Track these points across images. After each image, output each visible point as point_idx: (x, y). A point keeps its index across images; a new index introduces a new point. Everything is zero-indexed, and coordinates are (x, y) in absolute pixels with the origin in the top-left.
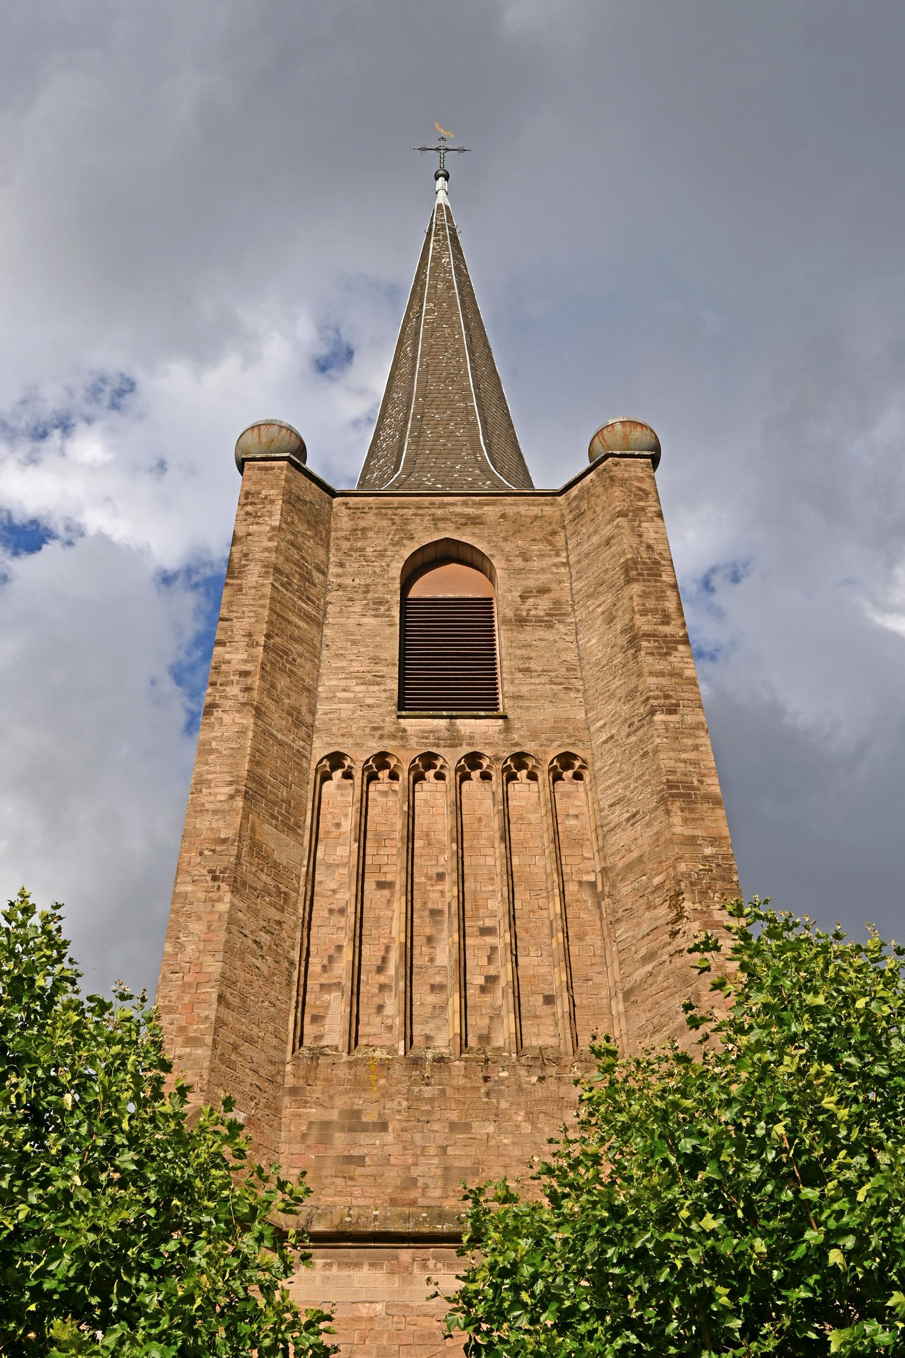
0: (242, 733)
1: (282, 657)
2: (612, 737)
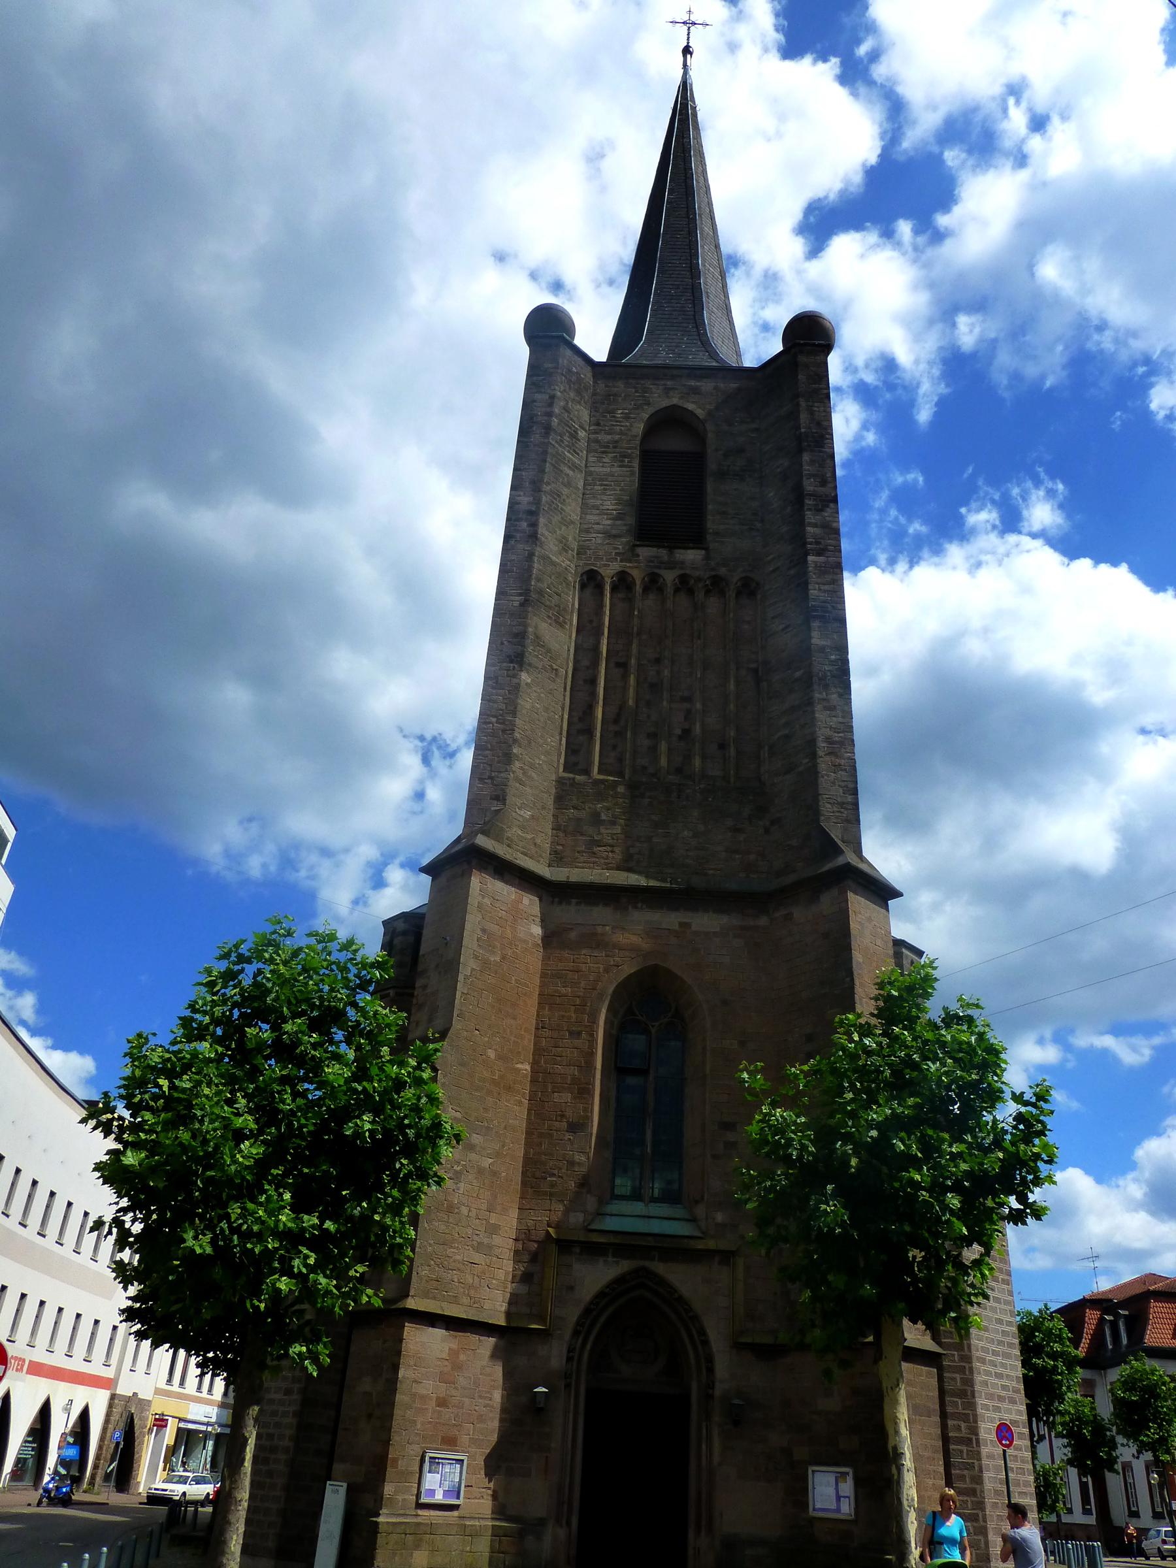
1: (556, 499)
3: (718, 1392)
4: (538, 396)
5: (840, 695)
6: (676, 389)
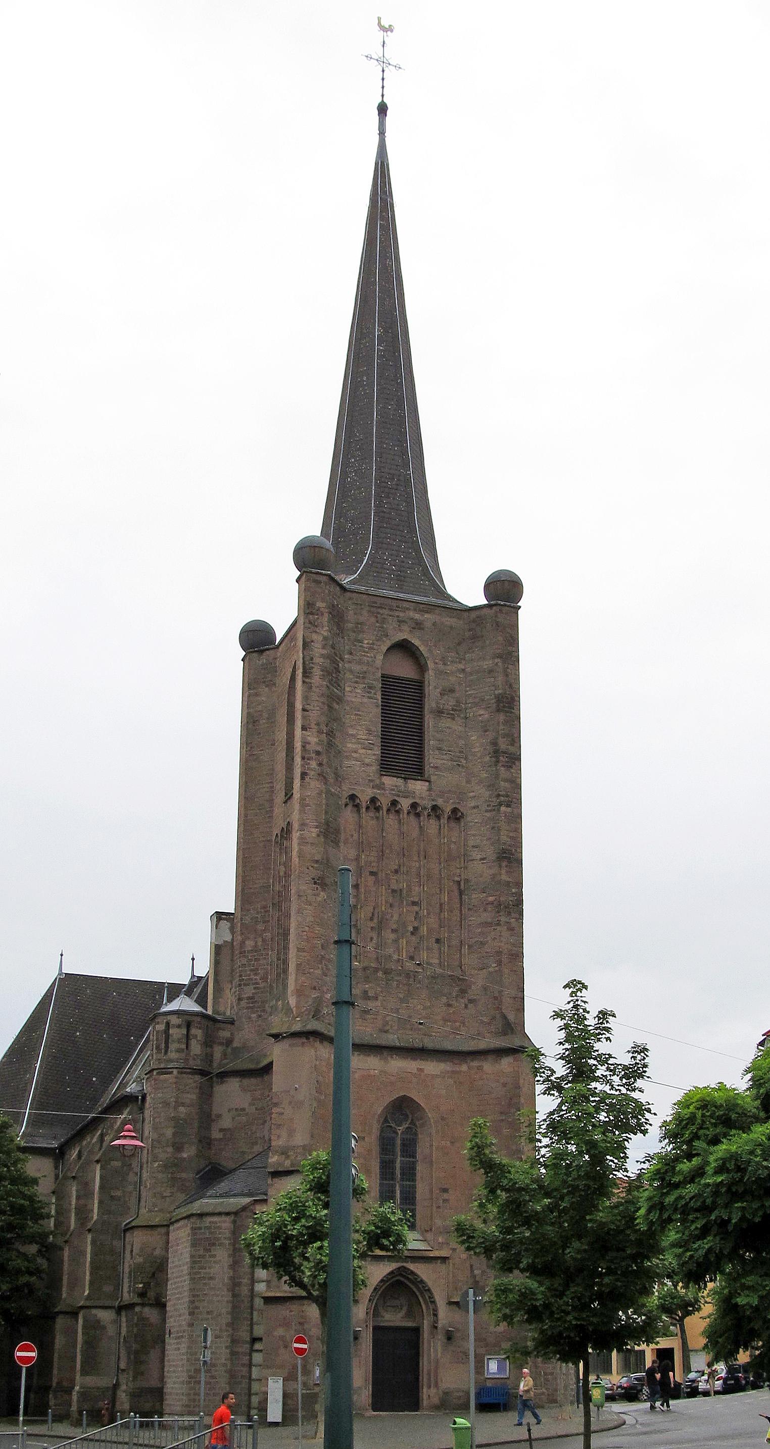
0: (320, 794)
2: (478, 807)
3: (440, 1325)
4: (315, 637)
5: (517, 919)
6: (406, 623)
